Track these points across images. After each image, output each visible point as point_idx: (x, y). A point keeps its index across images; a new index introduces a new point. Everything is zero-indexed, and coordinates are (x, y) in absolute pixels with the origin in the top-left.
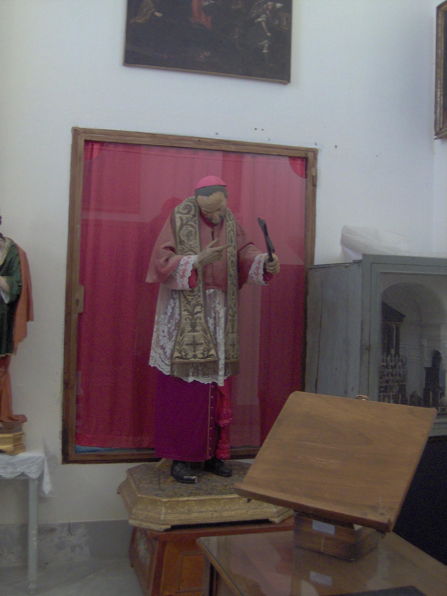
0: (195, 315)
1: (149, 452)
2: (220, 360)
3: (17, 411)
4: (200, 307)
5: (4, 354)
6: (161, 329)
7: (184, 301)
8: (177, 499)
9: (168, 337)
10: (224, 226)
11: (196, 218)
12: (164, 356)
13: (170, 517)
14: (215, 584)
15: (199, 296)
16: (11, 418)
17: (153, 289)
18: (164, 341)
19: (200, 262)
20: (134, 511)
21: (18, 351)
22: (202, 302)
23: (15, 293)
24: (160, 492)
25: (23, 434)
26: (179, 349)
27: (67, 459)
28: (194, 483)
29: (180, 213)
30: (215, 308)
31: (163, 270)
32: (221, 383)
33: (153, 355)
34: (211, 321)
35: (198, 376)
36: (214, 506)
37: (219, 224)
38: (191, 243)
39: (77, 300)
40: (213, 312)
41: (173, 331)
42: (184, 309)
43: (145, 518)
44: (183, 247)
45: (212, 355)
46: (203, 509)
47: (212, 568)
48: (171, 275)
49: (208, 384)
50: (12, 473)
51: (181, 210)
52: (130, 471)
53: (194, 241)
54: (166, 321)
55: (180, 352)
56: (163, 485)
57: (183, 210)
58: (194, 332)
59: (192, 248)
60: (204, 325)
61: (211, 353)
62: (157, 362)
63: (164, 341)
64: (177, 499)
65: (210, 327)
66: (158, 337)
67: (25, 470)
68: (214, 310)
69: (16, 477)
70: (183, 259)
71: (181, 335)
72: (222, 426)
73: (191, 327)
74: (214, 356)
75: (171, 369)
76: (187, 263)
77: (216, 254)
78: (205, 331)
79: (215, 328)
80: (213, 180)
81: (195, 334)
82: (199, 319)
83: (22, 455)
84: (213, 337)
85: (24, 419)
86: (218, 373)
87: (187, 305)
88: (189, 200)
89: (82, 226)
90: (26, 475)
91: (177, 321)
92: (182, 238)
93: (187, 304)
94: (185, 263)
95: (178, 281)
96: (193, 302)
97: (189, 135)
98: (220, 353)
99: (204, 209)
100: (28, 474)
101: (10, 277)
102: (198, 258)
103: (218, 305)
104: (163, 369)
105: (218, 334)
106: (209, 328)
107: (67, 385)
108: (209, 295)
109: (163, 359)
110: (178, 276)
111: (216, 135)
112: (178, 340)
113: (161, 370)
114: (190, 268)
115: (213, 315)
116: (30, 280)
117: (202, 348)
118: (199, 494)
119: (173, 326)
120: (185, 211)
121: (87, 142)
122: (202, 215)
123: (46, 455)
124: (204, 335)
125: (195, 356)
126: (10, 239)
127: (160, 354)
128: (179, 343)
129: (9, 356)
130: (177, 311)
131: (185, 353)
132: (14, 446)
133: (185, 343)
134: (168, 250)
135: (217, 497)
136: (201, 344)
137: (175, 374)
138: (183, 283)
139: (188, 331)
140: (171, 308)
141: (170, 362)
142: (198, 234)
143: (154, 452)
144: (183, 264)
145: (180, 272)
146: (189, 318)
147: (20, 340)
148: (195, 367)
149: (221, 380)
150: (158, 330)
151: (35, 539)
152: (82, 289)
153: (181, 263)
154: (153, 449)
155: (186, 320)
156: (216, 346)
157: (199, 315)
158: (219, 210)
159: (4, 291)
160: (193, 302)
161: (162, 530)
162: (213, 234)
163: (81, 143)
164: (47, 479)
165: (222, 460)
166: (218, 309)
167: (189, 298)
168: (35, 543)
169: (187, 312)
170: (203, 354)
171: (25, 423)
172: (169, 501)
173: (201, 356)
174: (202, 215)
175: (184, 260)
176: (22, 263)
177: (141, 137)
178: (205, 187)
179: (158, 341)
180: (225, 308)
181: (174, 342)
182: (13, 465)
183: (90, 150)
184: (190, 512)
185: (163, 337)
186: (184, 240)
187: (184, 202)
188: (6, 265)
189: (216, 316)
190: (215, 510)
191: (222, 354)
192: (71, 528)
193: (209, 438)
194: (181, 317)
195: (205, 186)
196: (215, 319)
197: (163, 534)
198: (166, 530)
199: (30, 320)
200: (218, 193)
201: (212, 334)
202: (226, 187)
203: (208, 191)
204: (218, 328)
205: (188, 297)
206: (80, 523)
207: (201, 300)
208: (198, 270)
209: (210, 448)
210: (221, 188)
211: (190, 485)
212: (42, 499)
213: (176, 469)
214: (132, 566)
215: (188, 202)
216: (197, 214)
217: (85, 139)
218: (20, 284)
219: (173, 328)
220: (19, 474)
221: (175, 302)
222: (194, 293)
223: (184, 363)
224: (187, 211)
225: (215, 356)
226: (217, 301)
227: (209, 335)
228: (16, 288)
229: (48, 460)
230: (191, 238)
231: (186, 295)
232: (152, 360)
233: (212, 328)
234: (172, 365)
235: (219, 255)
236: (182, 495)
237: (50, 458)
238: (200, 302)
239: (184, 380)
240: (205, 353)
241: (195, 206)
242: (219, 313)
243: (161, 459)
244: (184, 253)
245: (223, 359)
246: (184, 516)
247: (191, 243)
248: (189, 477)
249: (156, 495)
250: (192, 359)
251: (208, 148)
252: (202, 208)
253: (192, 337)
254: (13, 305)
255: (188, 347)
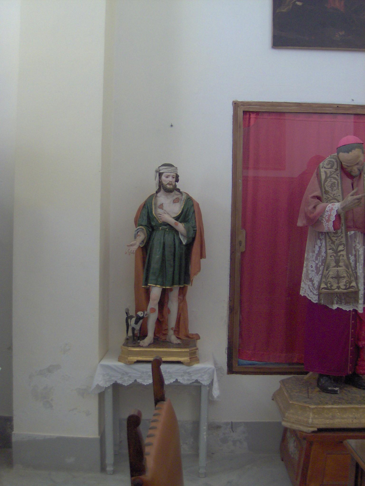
0: (338, 253)
1: (298, 367)
2: (360, 291)
3: (192, 330)
4: (343, 246)
5: (183, 285)
6: (310, 264)
7: (329, 241)
8: (322, 406)
9: (316, 271)
10: (362, 176)
11: (338, 171)
12: (312, 287)
13: (316, 421)
14: (359, 480)
15: (342, 237)
16: (188, 336)
17: (303, 232)
18: (312, 274)
19: (343, 208)
20: (287, 414)
21: (194, 282)
22: (344, 242)
23: (191, 235)
24: (308, 400)
25: (197, 349)
26: (325, 281)
27: (231, 370)
28: (337, 393)
29: (325, 168)
30: (355, 247)
31: (311, 216)
32: (360, 310)
33: (303, 287)
34: (352, 258)
35: (341, 304)
36: (354, 414)
37: (357, 176)
38: (335, 192)
39: (240, 241)
40: (353, 250)
41: (320, 266)
42: (329, 248)
43: (296, 421)
44: (328, 196)
45: (353, 286)
46: (344, 416)
47: (357, 466)
48: (318, 220)
49: (350, 311)
50: (188, 380)
51: (325, 166)
52: (283, 381)
53: (337, 191)
54: (314, 258)
55: (326, 284)
56: (311, 394)
57: (327, 165)
58: (337, 267)
59: (335, 197)
60: (347, 261)
61: (352, 285)
62: (306, 292)
63: (312, 274)
64: (322, 406)
65: (351, 263)
66: (307, 272)
67: (199, 378)
68: (354, 249)
69: (191, 383)
70: (328, 206)
71: (327, 270)
72: (361, 346)
73: (336, 264)
74: (355, 287)
75: (319, 298)
76: (332, 209)
77: (357, 201)
78: (347, 266)
79: (356, 264)
80: (351, 139)
81: (339, 268)
82: (342, 256)
83: (197, 366)
84: (354, 272)
85: (198, 337)
86: (358, 302)
87: (332, 245)
88: (332, 157)
89: (243, 180)
90: (199, 382)
91: (323, 258)
92: (327, 189)
93: (332, 244)
94: (330, 209)
95: (324, 224)
96: (337, 242)
97: (342, 103)
98: (359, 285)
99: (344, 164)
100: (201, 382)
101: (187, 224)
102: (341, 205)
103: (358, 245)
104: (312, 298)
105: (358, 269)
106: (350, 264)
107: (231, 309)
108: (351, 236)
109: (311, 290)
110: (324, 220)
111: (352, 101)
112: (324, 274)
113: (310, 299)
114: (334, 214)
115: (354, 252)
116: (202, 224)
117: (344, 281)
118: (341, 403)
119: (320, 262)
120: (329, 166)
121: (245, 113)
122: (342, 168)
123: (215, 367)
124: (347, 269)
125: (339, 288)
126: (186, 193)
127: (309, 285)
128: (325, 277)
129: (187, 287)
130: (323, 250)
131: (330, 285)
132: (190, 358)
133: (330, 276)
134: (315, 199)
135: (357, 406)
136: (344, 277)
137: (322, 302)
138: (328, 226)
139: (333, 266)
140: (318, 247)
141: (318, 292)
142: (340, 185)
143: (303, 366)
144: (328, 210)
145: (326, 217)
146: (333, 255)
147: (195, 274)
148: (338, 296)
149: (360, 307)
150: (307, 265)
151: (205, 433)
152: (244, 232)
153: (326, 209)
154: (303, 364)
155: (331, 257)
156: (356, 278)
157: (342, 253)
158: (357, 164)
159: (182, 235)
160: (337, 242)
161: (310, 431)
162: (352, 185)
163: (241, 114)
164: (216, 385)
165: (361, 375)
166: (358, 248)
167: (334, 239)
168: (205, 437)
169: (332, 250)
170: (345, 285)
171: (198, 340)
172: (316, 408)
173: (343, 287)
174: (342, 168)
175: (329, 207)
176: (196, 212)
177: (289, 106)
178: (345, 145)
179: (307, 275)
180: (364, 247)
181: (321, 275)
182: (189, 373)
183: (248, 119)
184: (334, 417)
185: (311, 271)
186: (328, 190)
187: (327, 159)
188: (184, 214)
189: (356, 254)
190: (354, 417)
191: (362, 286)
192: (233, 426)
193: (350, 357)
194: (327, 255)
195: (345, 144)
196: (355, 256)
197: (310, 435)
198: (314, 432)
199: (203, 258)
200: (357, 150)
201: (353, 269)
202: (363, 144)
203: (348, 148)
204: (358, 264)
205: (332, 238)
206: (241, 423)
207: (344, 240)
208: (341, 215)
209: (351, 365)
210: (359, 146)
211: (333, 395)
212: (211, 402)
213: (321, 381)
214: (282, 460)
215: (331, 158)
216: (339, 168)
217: (243, 110)
218: (195, 229)
219: (320, 264)
220: (193, 381)
221: (321, 242)
222: (337, 235)
223: (330, 293)
224: (331, 165)
225: (356, 287)
226: (357, 241)
227: (350, 270)
228: (192, 232)
229: (216, 370)
230: (335, 188)
231: (331, 236)
232: (302, 290)
233: (353, 264)
234: (319, 295)
235: (358, 202)
236: (327, 403)
237: (219, 369)
238: (342, 242)
239: (330, 307)
240: (347, 284)
241: (337, 161)
242: (359, 251)
243: (309, 372)
244: (328, 201)
245: (362, 290)
246: (328, 420)
247: (335, 192)
248: (332, 388)
249: (305, 402)
250: (337, 290)
251: (346, 113)
252: (343, 163)
253: (336, 271)
254: (189, 246)
255: (333, 280)
